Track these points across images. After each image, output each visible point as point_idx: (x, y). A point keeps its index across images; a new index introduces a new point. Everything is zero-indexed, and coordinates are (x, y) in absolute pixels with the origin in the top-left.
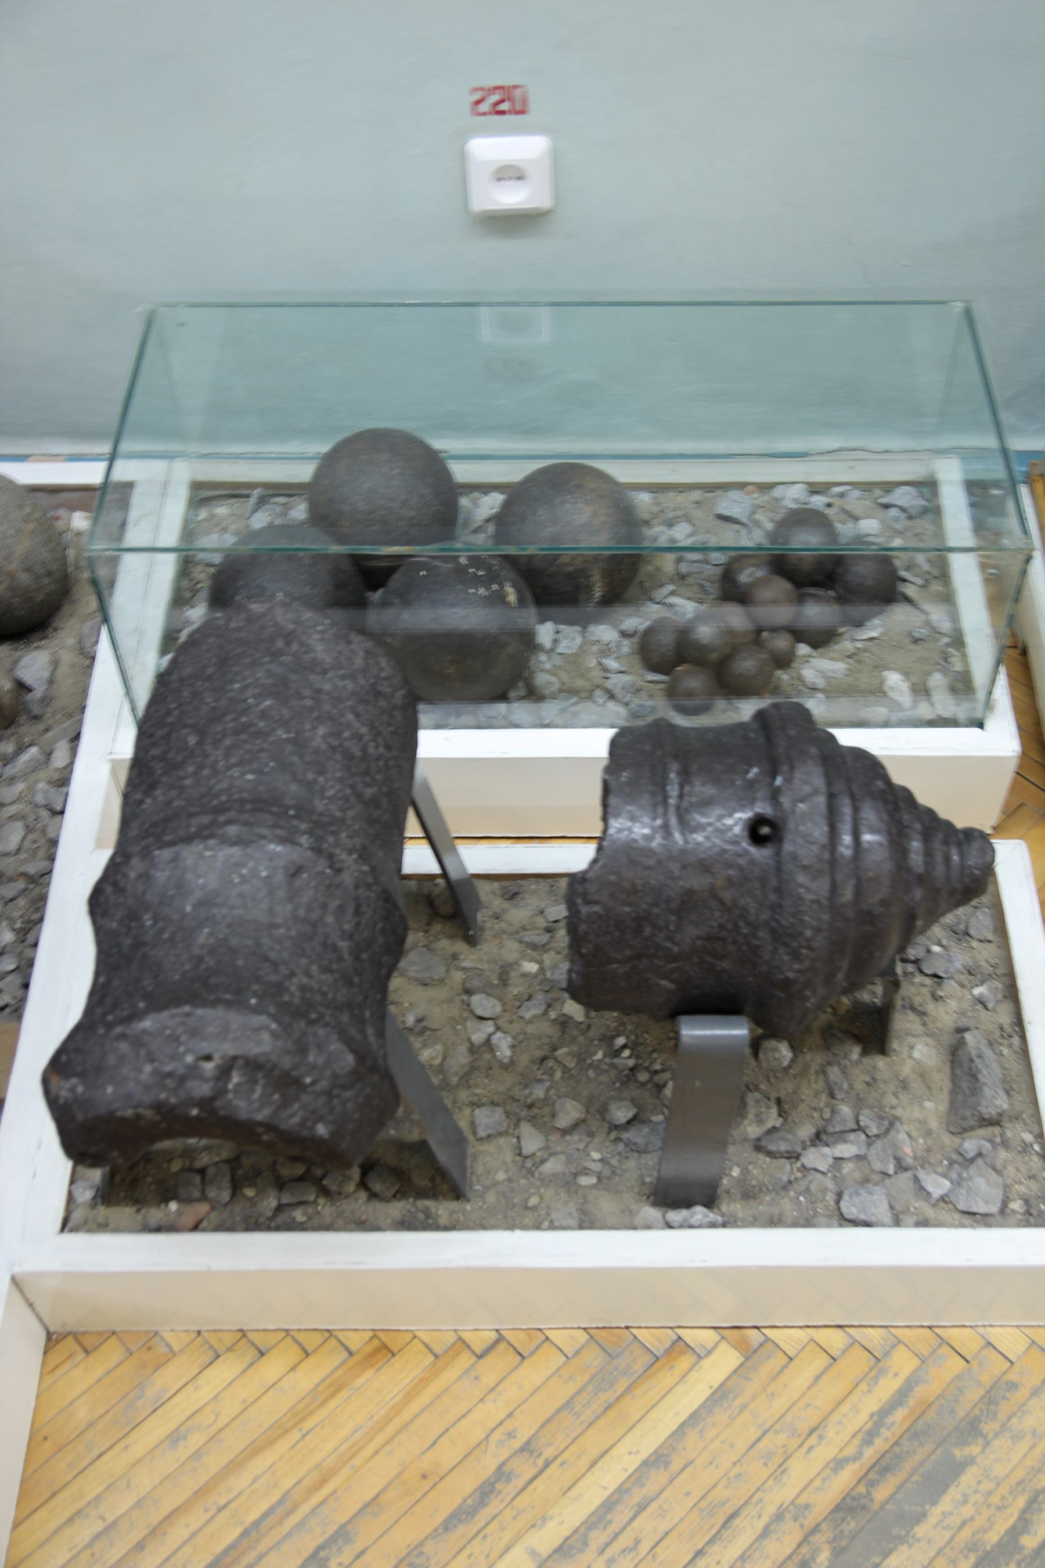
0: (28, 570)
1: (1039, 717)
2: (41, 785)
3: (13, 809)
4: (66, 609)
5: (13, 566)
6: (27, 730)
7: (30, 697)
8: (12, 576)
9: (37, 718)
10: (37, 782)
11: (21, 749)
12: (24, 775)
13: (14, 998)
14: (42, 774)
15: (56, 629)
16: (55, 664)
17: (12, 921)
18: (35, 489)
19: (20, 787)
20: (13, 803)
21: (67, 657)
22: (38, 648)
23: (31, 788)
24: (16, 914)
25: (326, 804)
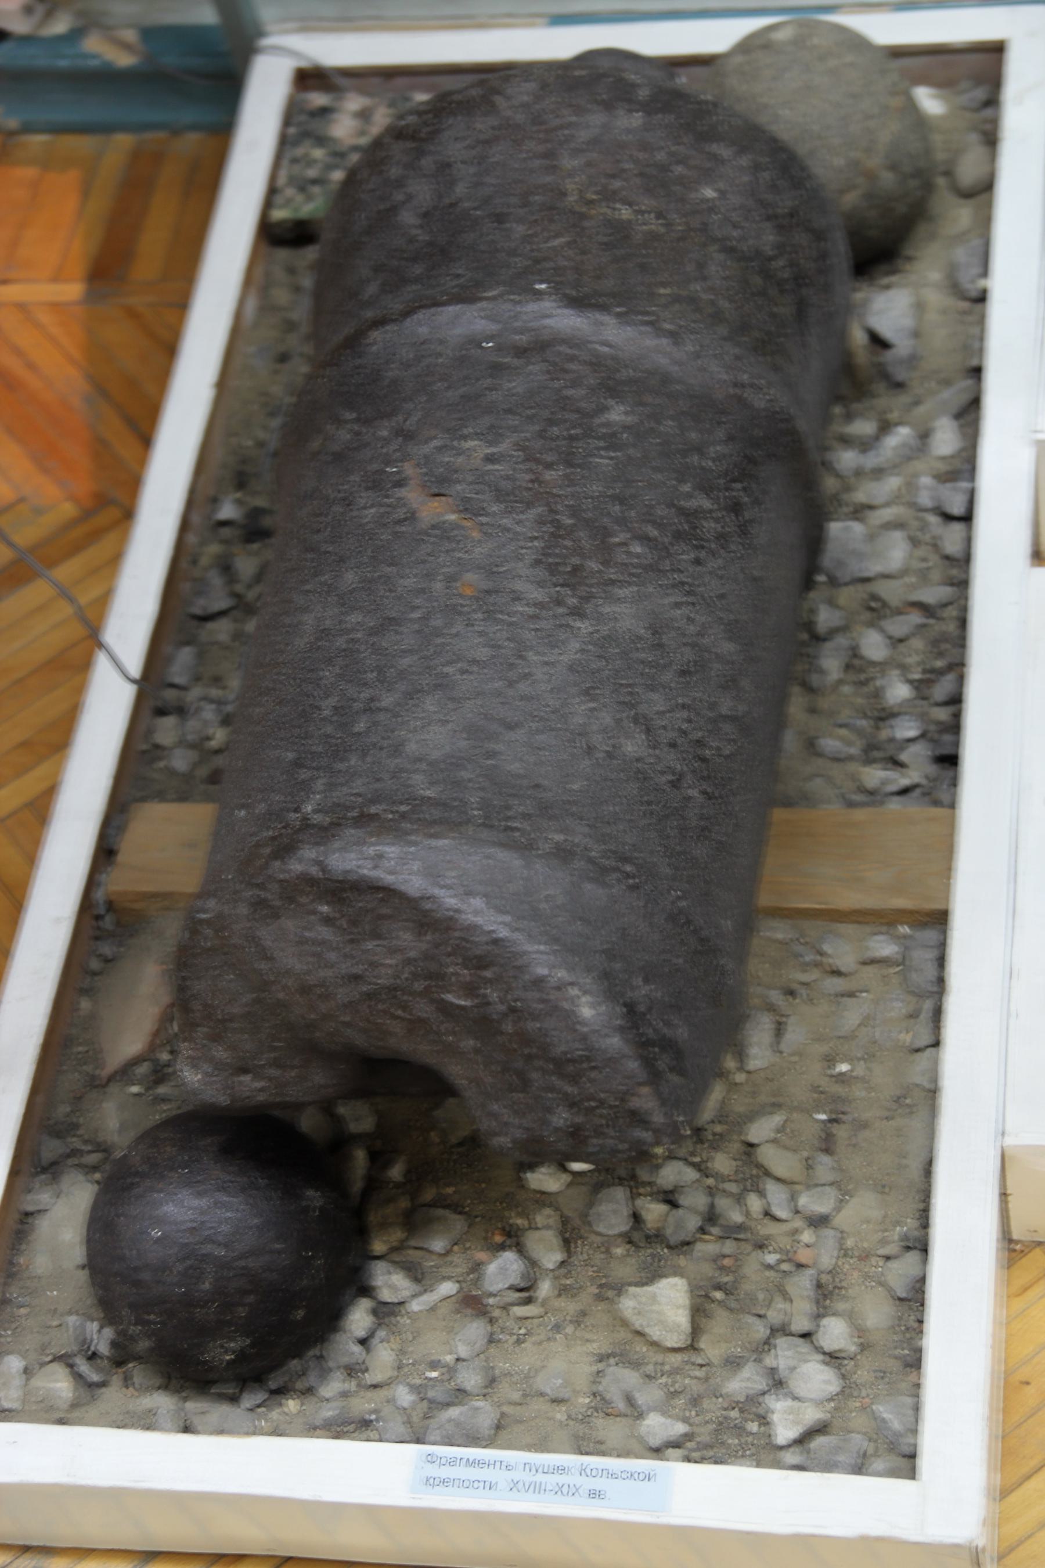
0: (893, 167)
1: (1006, 1399)
2: (926, 481)
3: (887, 514)
4: (922, 229)
5: (874, 162)
6: (894, 404)
7: (888, 356)
8: (871, 176)
9: (899, 386)
10: (916, 475)
11: (885, 427)
12: (894, 467)
13: (927, 777)
14: (918, 465)
15: (909, 259)
16: (920, 307)
17: (904, 668)
18: (898, 52)
19: (893, 483)
20: (887, 505)
21: (936, 298)
22: (888, 287)
23: (911, 485)
24: (912, 660)
25: (714, 755)
